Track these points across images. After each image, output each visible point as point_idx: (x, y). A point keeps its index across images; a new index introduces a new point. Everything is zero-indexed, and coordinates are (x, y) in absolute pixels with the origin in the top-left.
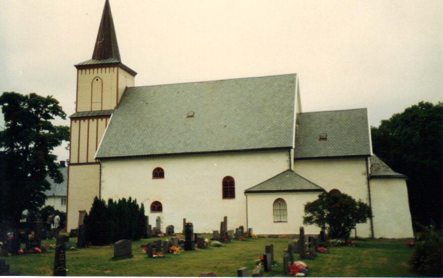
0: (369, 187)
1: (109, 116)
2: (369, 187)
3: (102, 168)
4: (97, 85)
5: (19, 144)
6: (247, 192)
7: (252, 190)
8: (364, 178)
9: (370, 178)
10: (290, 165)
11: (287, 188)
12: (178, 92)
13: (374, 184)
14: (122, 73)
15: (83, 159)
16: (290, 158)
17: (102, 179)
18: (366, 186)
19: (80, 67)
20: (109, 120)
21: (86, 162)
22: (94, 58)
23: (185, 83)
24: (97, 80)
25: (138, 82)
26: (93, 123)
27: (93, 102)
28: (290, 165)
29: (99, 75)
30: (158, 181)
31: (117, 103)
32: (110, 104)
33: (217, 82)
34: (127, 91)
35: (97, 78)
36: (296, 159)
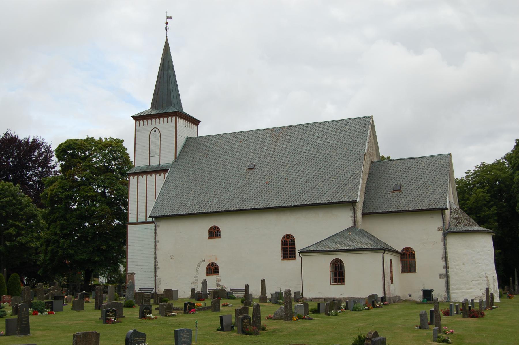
0: (445, 245)
1: (167, 170)
2: (445, 245)
3: (157, 228)
4: (155, 136)
5: (461, 185)
6: (301, 252)
7: (307, 250)
8: (440, 234)
9: (447, 233)
10: (355, 221)
11: (345, 248)
12: (241, 142)
13: (451, 240)
14: (182, 124)
15: (142, 219)
16: (354, 213)
17: (157, 240)
18: (442, 244)
19: (137, 118)
20: (167, 174)
21: (145, 221)
22: (152, 107)
23: (248, 131)
24: (155, 131)
25: (203, 131)
26: (151, 178)
27: (159, 156)
28: (355, 221)
29: (157, 126)
30: (215, 241)
31: (176, 158)
32: (168, 159)
33: (282, 128)
34: (451, 203)
35: (157, 130)
36: (364, 214)
